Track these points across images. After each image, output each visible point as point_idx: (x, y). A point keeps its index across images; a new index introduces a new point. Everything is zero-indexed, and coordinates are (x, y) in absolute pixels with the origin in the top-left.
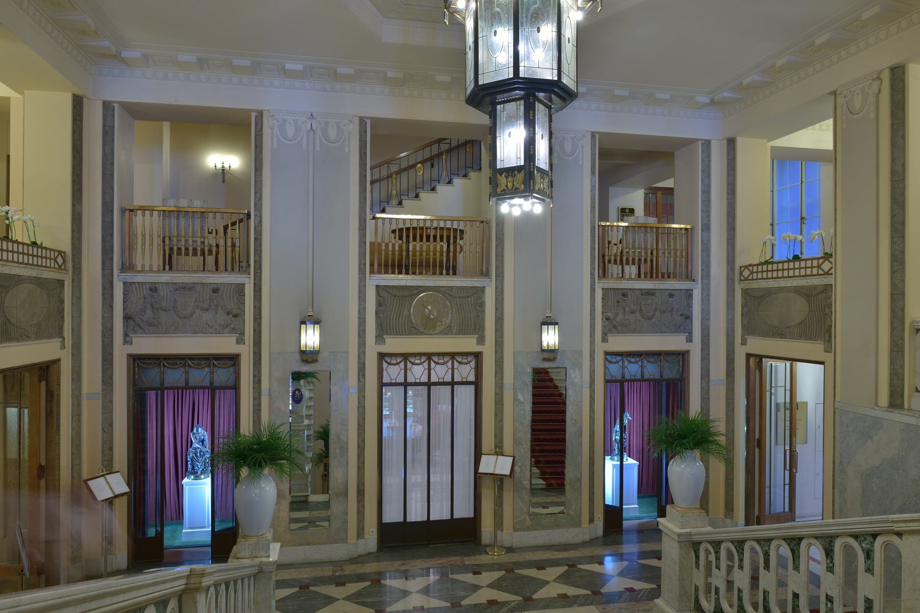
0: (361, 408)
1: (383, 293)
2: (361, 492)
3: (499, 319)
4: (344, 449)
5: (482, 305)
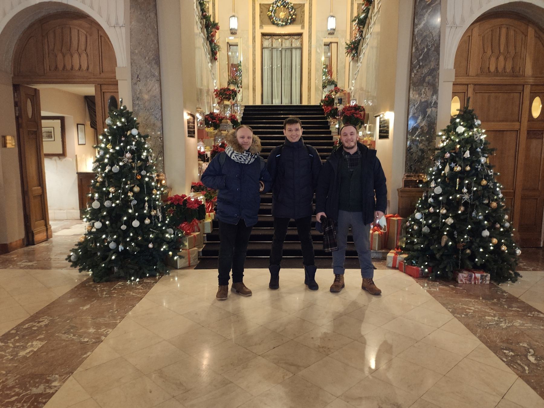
0: (254, 55)
1: (262, 7)
2: (254, 90)
3: (310, 17)
4: (247, 70)
5: (303, 12)
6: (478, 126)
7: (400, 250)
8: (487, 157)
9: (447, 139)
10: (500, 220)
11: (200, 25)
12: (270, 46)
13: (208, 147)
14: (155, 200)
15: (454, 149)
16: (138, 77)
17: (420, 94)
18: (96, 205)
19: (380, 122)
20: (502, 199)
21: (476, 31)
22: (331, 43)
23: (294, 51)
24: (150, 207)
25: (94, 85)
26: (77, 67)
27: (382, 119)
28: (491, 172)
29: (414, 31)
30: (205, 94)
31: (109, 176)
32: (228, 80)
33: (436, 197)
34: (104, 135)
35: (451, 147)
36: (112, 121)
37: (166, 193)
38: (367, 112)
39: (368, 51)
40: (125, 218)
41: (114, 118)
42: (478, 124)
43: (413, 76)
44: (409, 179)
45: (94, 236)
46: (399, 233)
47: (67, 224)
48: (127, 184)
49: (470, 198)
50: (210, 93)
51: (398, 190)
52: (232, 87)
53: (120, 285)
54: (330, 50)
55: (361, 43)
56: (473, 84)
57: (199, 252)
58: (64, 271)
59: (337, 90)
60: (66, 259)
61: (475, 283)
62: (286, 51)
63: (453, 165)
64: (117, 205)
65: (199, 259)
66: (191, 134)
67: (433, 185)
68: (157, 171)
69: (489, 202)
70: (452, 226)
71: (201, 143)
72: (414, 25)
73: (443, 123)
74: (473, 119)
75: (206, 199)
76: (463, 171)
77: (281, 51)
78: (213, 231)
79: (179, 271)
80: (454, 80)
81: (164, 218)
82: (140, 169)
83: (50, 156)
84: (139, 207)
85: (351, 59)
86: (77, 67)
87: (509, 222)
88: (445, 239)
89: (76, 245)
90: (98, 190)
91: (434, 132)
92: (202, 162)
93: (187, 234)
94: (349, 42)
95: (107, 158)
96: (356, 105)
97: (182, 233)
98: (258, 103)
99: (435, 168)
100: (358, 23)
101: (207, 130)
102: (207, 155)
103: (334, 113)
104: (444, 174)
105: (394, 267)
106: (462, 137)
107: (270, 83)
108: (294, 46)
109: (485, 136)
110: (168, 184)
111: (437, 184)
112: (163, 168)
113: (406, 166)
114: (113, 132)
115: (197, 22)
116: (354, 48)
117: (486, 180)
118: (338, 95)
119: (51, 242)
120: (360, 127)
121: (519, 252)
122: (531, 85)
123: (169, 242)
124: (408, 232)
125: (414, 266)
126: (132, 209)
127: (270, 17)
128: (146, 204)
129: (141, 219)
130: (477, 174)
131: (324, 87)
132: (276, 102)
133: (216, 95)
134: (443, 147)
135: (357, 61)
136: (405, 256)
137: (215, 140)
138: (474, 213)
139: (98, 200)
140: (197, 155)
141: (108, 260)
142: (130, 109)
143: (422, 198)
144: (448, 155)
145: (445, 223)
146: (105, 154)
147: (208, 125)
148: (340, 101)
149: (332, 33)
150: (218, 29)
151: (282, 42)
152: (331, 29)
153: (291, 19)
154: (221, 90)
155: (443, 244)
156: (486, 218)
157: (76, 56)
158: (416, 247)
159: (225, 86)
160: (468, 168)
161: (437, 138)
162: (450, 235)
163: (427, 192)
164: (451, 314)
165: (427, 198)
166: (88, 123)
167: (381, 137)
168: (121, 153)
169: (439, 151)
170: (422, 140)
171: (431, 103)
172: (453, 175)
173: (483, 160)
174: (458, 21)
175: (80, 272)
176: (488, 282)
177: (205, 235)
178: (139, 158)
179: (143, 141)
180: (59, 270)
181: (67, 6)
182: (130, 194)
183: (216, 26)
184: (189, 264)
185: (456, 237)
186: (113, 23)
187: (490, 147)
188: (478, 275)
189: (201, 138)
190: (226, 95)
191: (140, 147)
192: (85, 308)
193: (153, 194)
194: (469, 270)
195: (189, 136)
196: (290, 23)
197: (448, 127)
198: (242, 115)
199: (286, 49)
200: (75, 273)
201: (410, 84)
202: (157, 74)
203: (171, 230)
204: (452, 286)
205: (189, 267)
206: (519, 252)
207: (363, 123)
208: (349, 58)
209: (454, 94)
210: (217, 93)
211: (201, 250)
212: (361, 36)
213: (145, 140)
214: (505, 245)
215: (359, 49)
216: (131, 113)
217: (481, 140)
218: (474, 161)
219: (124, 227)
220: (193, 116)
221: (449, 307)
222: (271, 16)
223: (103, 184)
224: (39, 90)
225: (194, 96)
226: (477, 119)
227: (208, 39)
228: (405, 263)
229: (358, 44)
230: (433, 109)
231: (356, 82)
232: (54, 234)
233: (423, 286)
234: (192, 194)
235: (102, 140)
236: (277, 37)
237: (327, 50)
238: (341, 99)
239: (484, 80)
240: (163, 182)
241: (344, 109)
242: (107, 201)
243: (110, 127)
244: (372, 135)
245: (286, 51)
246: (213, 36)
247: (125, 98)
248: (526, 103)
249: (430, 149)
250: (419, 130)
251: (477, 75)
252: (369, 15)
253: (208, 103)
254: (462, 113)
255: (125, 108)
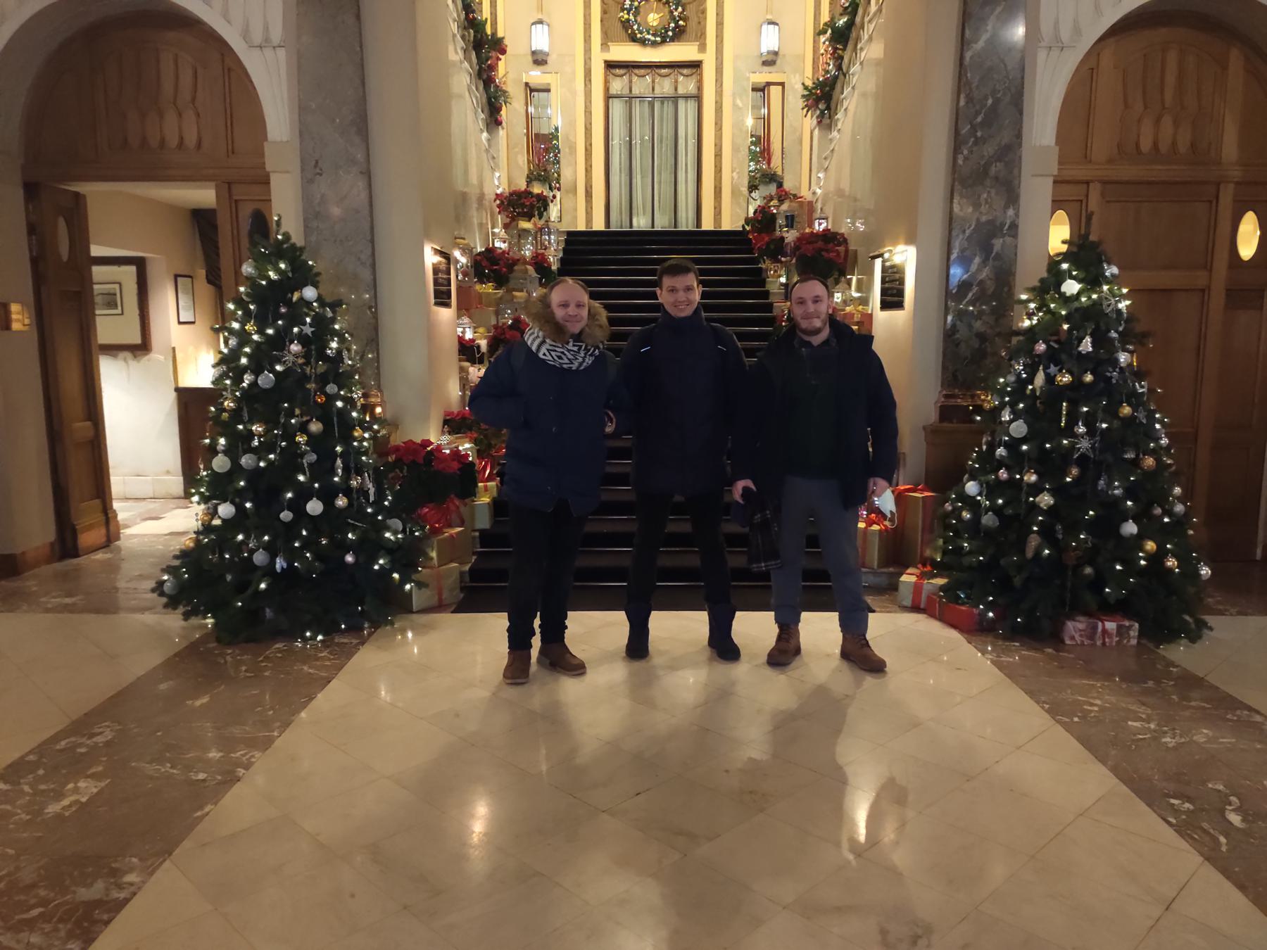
2: (589, 194)
3: (720, 24)
4: (573, 149)
5: (704, 12)
6: (1112, 280)
7: (929, 568)
8: (1131, 352)
9: (1039, 309)
10: (1163, 499)
11: (461, 43)
12: (626, 92)
13: (481, 330)
14: (360, 452)
15: (1057, 331)
16: (316, 166)
17: (977, 206)
18: (221, 463)
19: (884, 270)
20: (1168, 448)
21: (1107, 59)
22: (769, 84)
23: (681, 103)
24: (346, 469)
25: (213, 184)
26: (173, 142)
27: (888, 264)
28: (1142, 387)
29: (962, 58)
30: (475, 206)
31: (252, 397)
32: (526, 172)
33: (1013, 445)
34: (240, 303)
35: (1047, 329)
36: (256, 268)
37: (384, 436)
38: (852, 247)
39: (855, 105)
40: (289, 495)
41: (262, 262)
42: (1113, 275)
43: (960, 162)
44: (952, 402)
45: (214, 537)
46: (928, 529)
47: (153, 505)
48: (293, 416)
49: (1093, 448)
50: (486, 203)
51: (924, 428)
52: (537, 189)
53: (280, 651)
54: (766, 101)
55: (838, 85)
56: (1100, 181)
57: (462, 574)
58: (149, 618)
59: (783, 196)
60: (153, 590)
61: (1104, 644)
62: (662, 103)
63: (1053, 369)
64: (270, 463)
65: (462, 589)
66: (442, 298)
67: (1006, 416)
68: (362, 384)
69: (1137, 455)
70: (1051, 511)
71: (466, 320)
72: (963, 43)
73: (1030, 272)
74: (1101, 262)
75: (478, 451)
76: (1077, 384)
77: (652, 105)
78: (495, 523)
79: (415, 616)
80: (1056, 173)
81: (380, 495)
82: (323, 380)
83: (113, 350)
84: (322, 469)
85: (815, 122)
86: (173, 142)
87: (1185, 504)
88: (1034, 541)
89: (176, 557)
90: (226, 428)
91: (1011, 293)
92: (466, 364)
93: (436, 532)
94: (809, 83)
95: (247, 355)
96: (826, 230)
97: (423, 528)
98: (599, 225)
99: (1012, 378)
100: (831, 40)
101: (480, 288)
102: (479, 347)
103: (776, 250)
104: (1033, 390)
105: (915, 608)
106: (1076, 304)
107: (625, 178)
108: (681, 91)
109: (1128, 302)
110: (388, 416)
111: (1016, 415)
112: (378, 376)
113: (943, 374)
114: (258, 294)
115: (454, 36)
116: (823, 97)
117: (1129, 405)
118: (785, 207)
119: (119, 549)
120: (837, 282)
121: (1205, 571)
122: (1237, 183)
123: (391, 550)
124: (948, 527)
125: (963, 604)
126: (304, 474)
127: (626, 25)
128: (339, 462)
129: (327, 496)
130: (1109, 391)
131: (752, 187)
132: (641, 223)
133: (499, 206)
134: (1032, 328)
135: (829, 128)
136: (941, 581)
137: (497, 313)
138: (1102, 482)
139: (226, 452)
140: (455, 346)
141: (250, 591)
142: (298, 239)
143: (980, 448)
144: (1041, 347)
145: (1035, 506)
146: (241, 345)
147: (482, 278)
148: (791, 221)
149: (770, 61)
150: (503, 52)
151: (653, 82)
152: (769, 52)
153: (673, 30)
154: (511, 194)
155: (1030, 554)
156: (1130, 492)
157: (171, 119)
158: (967, 561)
159: (522, 185)
160: (1089, 378)
161: (1016, 307)
162: (1047, 534)
163: (993, 434)
164: (1047, 716)
165: (992, 447)
166: (201, 273)
167: (885, 306)
168: (280, 342)
169: (1021, 338)
170: (981, 313)
171: (1003, 225)
172: (1054, 392)
173: (1123, 358)
174: (1065, 34)
175: (186, 620)
176: (1134, 642)
177: (477, 534)
178: (322, 356)
179: (330, 315)
180: (139, 616)
181: (185, 10)
182: (301, 439)
183: (498, 46)
184: (440, 600)
185: (1060, 537)
186: (257, 38)
187: (1139, 328)
188: (1111, 626)
189: (465, 308)
190: (521, 207)
191: (323, 329)
192: (198, 703)
193: (355, 439)
194: (1088, 614)
195: (437, 304)
196: (672, 39)
197: (1042, 281)
198: (561, 255)
199: (663, 99)
200: (174, 621)
201: (954, 180)
202: (360, 156)
203: (397, 523)
204: (1050, 650)
205: (439, 607)
206: (1205, 571)
207: (843, 273)
208: (810, 122)
209: (1057, 204)
210: (502, 202)
211: (467, 568)
212: (839, 68)
213: (334, 312)
214: (1174, 556)
215: (835, 98)
216: (302, 249)
217: (1119, 312)
218: (1102, 360)
219: (286, 516)
220: (446, 256)
221: (1043, 698)
222: (628, 20)
223: (236, 415)
224: (84, 196)
225: (450, 210)
226: (1109, 264)
227: (479, 74)
228: (941, 597)
229: (833, 87)
230: (1008, 240)
231: (827, 174)
232: (126, 532)
233: (984, 652)
234: (445, 439)
235: (234, 313)
236: (642, 71)
237: (760, 102)
238: (793, 217)
239: (1128, 172)
240: (379, 410)
241: (799, 239)
242: (247, 456)
243: (251, 281)
244: (864, 301)
245: (662, 103)
246: (493, 68)
247: (287, 215)
248: (1224, 226)
249: (999, 334)
250: (975, 289)
251: (1110, 161)
252: (858, 19)
253: (481, 225)
254: (1075, 249)
255: (287, 237)
